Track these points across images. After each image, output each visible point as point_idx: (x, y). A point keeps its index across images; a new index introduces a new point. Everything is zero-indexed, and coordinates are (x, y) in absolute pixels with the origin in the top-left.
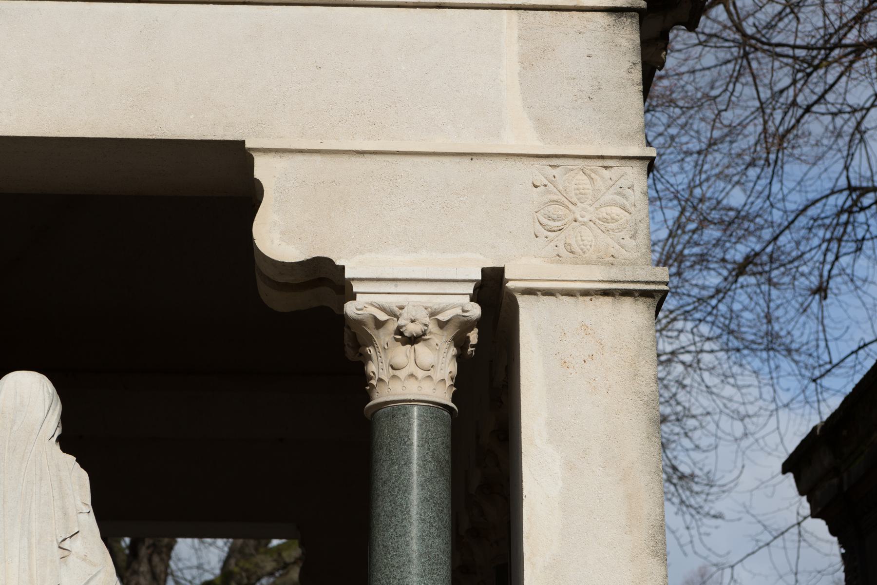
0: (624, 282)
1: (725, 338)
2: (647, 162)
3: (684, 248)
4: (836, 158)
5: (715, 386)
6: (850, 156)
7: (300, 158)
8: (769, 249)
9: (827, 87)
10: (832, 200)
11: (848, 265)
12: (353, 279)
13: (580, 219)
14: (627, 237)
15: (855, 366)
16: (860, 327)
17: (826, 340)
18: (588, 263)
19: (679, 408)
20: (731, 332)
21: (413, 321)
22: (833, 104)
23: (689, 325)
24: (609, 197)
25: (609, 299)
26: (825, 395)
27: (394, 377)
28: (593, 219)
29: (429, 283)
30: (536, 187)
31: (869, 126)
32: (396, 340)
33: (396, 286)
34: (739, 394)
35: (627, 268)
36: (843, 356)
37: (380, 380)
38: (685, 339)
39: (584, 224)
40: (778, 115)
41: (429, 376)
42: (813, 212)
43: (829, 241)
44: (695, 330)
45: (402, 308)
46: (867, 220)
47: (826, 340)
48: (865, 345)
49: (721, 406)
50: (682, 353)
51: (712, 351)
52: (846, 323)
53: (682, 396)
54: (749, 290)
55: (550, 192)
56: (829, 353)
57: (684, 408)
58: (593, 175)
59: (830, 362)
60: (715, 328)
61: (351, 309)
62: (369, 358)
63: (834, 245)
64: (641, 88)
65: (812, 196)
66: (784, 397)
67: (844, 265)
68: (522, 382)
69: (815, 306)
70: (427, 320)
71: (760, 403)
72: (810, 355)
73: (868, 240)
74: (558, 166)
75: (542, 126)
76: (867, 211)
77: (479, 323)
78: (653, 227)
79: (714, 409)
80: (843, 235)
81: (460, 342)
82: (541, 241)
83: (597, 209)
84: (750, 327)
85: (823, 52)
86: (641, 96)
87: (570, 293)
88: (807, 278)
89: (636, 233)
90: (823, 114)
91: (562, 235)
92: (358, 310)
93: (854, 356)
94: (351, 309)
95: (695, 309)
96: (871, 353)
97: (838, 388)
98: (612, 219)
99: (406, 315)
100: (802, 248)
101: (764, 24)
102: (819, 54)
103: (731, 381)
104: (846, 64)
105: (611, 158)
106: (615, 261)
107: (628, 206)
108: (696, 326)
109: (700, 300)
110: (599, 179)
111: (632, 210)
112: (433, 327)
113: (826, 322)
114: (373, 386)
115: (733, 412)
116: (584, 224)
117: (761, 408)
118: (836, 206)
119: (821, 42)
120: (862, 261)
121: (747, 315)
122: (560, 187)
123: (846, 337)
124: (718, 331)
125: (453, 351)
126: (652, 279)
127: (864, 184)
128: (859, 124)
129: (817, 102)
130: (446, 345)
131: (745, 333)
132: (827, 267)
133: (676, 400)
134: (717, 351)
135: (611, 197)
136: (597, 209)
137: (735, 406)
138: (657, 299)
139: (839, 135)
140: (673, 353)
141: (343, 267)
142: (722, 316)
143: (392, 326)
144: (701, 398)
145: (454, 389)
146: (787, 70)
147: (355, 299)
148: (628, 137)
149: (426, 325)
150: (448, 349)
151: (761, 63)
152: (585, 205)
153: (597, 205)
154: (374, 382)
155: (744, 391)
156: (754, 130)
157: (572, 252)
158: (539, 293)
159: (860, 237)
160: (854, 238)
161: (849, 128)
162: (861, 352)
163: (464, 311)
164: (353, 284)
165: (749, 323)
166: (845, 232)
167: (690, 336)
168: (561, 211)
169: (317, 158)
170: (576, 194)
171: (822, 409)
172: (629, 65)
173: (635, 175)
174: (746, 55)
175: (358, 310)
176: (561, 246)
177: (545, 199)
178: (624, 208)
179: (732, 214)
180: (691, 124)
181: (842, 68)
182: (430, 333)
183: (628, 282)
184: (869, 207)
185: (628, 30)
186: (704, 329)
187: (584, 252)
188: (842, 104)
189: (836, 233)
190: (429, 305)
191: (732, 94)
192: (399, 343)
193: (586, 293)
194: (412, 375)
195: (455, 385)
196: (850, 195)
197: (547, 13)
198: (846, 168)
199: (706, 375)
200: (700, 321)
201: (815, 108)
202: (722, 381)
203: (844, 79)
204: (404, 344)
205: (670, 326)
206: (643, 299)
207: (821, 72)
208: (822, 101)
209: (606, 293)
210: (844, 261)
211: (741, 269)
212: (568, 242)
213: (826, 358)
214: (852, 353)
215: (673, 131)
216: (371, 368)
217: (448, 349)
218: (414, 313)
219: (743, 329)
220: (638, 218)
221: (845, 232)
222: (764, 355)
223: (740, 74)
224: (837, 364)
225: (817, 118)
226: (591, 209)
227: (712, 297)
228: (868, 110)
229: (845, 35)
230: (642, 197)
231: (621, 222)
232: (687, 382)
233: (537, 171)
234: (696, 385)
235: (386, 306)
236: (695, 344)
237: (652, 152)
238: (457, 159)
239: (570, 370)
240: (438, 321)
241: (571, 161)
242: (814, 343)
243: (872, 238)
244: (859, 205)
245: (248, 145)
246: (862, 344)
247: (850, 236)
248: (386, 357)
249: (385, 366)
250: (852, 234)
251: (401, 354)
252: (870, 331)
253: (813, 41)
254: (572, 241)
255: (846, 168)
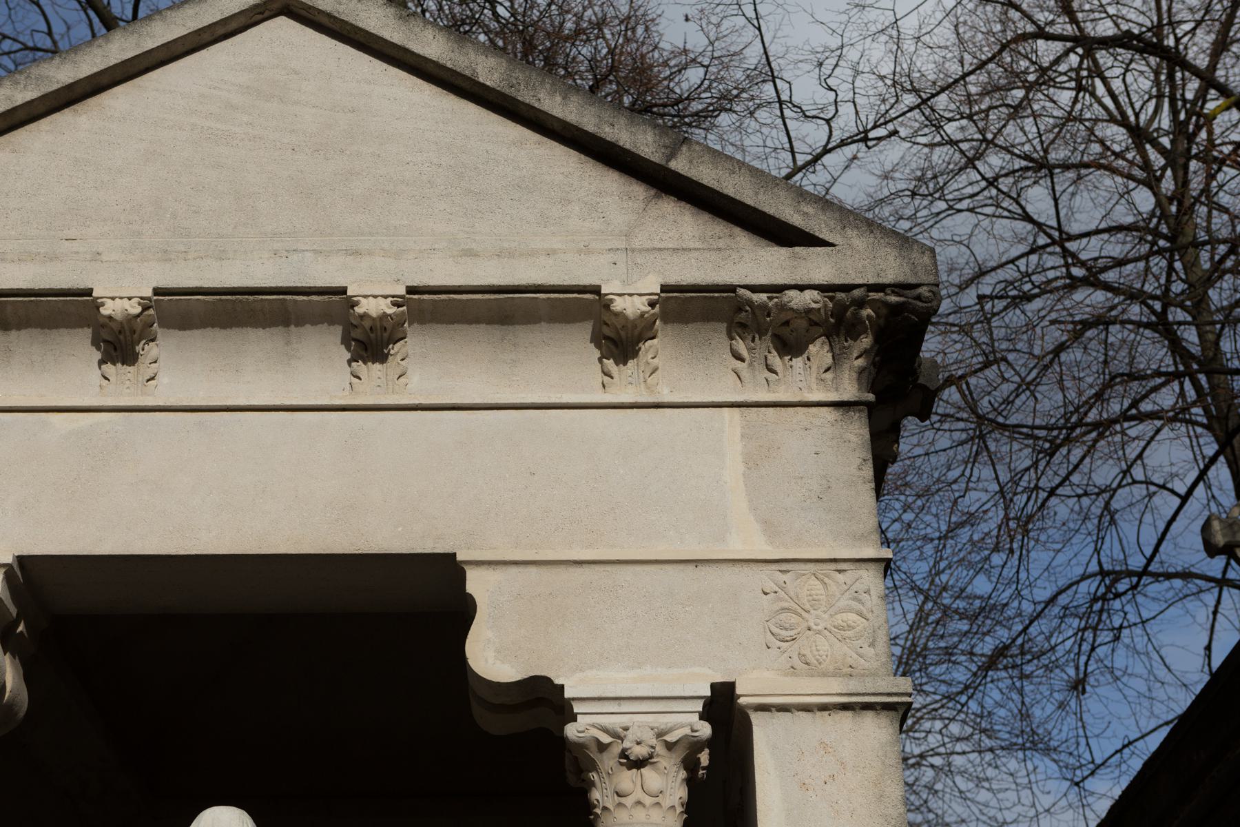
0: (864, 694)
1: (976, 737)
2: (883, 565)
3: (928, 640)
4: (1085, 543)
5: (969, 791)
6: (1100, 540)
7: (514, 570)
8: (1020, 641)
9: (1071, 467)
10: (1083, 587)
11: (1106, 656)
12: (574, 699)
13: (815, 627)
14: (865, 646)
15: (1120, 765)
16: (1122, 724)
17: (1086, 737)
18: (825, 675)
19: (931, 816)
20: (983, 731)
21: (638, 743)
22: (1078, 486)
23: (938, 725)
24: (843, 603)
25: (849, 714)
26: (1090, 799)
27: (620, 805)
28: (829, 626)
29: (655, 701)
30: (766, 594)
31: (1118, 508)
32: (622, 764)
33: (619, 705)
34: (995, 799)
35: (868, 679)
36: (1107, 755)
37: (605, 808)
38: (933, 740)
39: (819, 632)
40: (1020, 500)
41: (658, 804)
42: (1063, 600)
43: (1085, 629)
44: (944, 731)
45: (626, 729)
46: (1123, 606)
47: (1086, 737)
48: (1130, 743)
49: (977, 812)
50: (932, 756)
51: (964, 753)
52: (1107, 719)
53: (933, 803)
54: (1000, 685)
55: (781, 599)
56: (1091, 752)
57: (937, 815)
58: (826, 580)
59: (1093, 762)
60: (966, 727)
61: (571, 731)
62: (593, 784)
63: (1089, 635)
64: (873, 485)
65: (1062, 583)
66: (1046, 801)
67: (1102, 656)
68: (758, 807)
69: (1073, 703)
70: (654, 742)
71: (1019, 809)
72: (1071, 754)
73: (1125, 628)
74: (789, 571)
75: (770, 528)
76: (1123, 598)
77: (710, 743)
78: (893, 621)
79: (969, 816)
80: (1098, 624)
81: (690, 764)
82: (774, 652)
83: (831, 616)
84: (1004, 724)
85: (1064, 431)
86: (873, 494)
87: (806, 708)
88: (1063, 670)
89: (874, 640)
90: (1069, 497)
91: (796, 645)
92: (579, 732)
93: (1118, 755)
94: (571, 731)
95: (943, 706)
96: (1137, 752)
97: (1103, 792)
98: (849, 626)
99: (631, 736)
100: (1053, 641)
101: (1000, 400)
102: (1060, 433)
103: (986, 785)
104: (1090, 443)
105: (845, 560)
106: (854, 672)
107: (865, 612)
108: (946, 726)
109: (949, 698)
110: (832, 584)
111: (869, 616)
112: (660, 749)
113: (1085, 716)
114: (597, 816)
115: (990, 818)
116: (819, 632)
117: (1019, 815)
118: (1089, 593)
119: (1062, 421)
120: (1121, 651)
121: (1002, 712)
122: (792, 594)
123: (1109, 733)
124: (969, 730)
125: (683, 774)
126: (894, 690)
127: (1118, 568)
128: (1107, 504)
129: (1061, 484)
130: (675, 769)
131: (999, 731)
132: (1083, 659)
133: (928, 807)
134: (969, 752)
135: (846, 602)
136: (831, 616)
137: (992, 812)
138: (901, 713)
139: (1086, 518)
140: (922, 756)
141: (562, 686)
142: (973, 713)
143: (616, 750)
144: (954, 805)
145: (685, 816)
146: (1028, 451)
147: (575, 720)
148: (862, 538)
149: (653, 747)
150: (678, 772)
151: (998, 444)
152: (819, 612)
153: (832, 611)
154: (598, 811)
155: (1000, 796)
156: (997, 515)
157: (807, 664)
158: (773, 709)
159: (1117, 625)
160: (1110, 626)
161: (1096, 510)
162: (1126, 751)
163: (693, 731)
164: (574, 703)
165: (1002, 720)
166: (1100, 620)
167: (939, 737)
168: (794, 619)
169: (533, 570)
170: (809, 601)
171: (1087, 813)
172: (859, 461)
173: (870, 579)
174: (982, 437)
175: (579, 732)
176: (795, 657)
177: (776, 607)
178: (861, 615)
179: (977, 603)
180: (929, 507)
181: (1085, 448)
182: (658, 755)
183: (868, 694)
184: (1125, 593)
185: (857, 425)
186: (955, 728)
187: (820, 663)
188: (1087, 485)
189: (1090, 621)
190: (656, 725)
191: (969, 479)
192: (624, 768)
193: (824, 708)
194: (639, 803)
195: (686, 812)
196: (1103, 580)
197: (771, 410)
198: (1097, 551)
199: (958, 779)
200: (950, 720)
201: (1060, 491)
202: (977, 786)
203: (1087, 460)
204: (629, 769)
205: (917, 727)
206: (886, 712)
207: (1064, 451)
208: (1067, 483)
209: (845, 707)
210: (1101, 651)
211: (992, 662)
212: (803, 652)
213: (1087, 756)
214: (1117, 752)
215: (908, 516)
216: (596, 795)
217: (678, 772)
218: (639, 735)
219: (996, 727)
220: (877, 625)
221: (1100, 620)
222: (1020, 754)
223: (977, 454)
224: (1103, 764)
225: (1063, 501)
226: (826, 616)
227: (961, 693)
228: (1115, 490)
229: (1086, 414)
230: (879, 601)
231: (857, 629)
232: (938, 786)
233: (767, 577)
234: (948, 790)
235: (609, 727)
236: (944, 745)
237: (887, 553)
238: (681, 567)
239: (810, 793)
240: (665, 741)
241: (802, 566)
242: (1073, 740)
243: (1130, 626)
244: (1113, 590)
245: (459, 558)
246: (1126, 742)
247: (1105, 624)
248: (611, 783)
249: (610, 792)
250: (1108, 621)
251: (627, 779)
252: (1134, 727)
253: (1053, 421)
254: (807, 652)
255: (1097, 551)
